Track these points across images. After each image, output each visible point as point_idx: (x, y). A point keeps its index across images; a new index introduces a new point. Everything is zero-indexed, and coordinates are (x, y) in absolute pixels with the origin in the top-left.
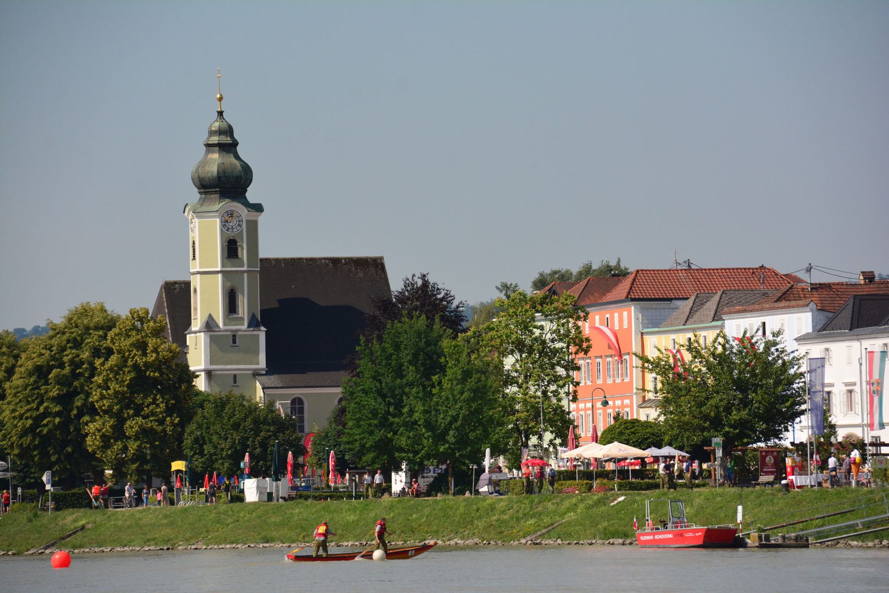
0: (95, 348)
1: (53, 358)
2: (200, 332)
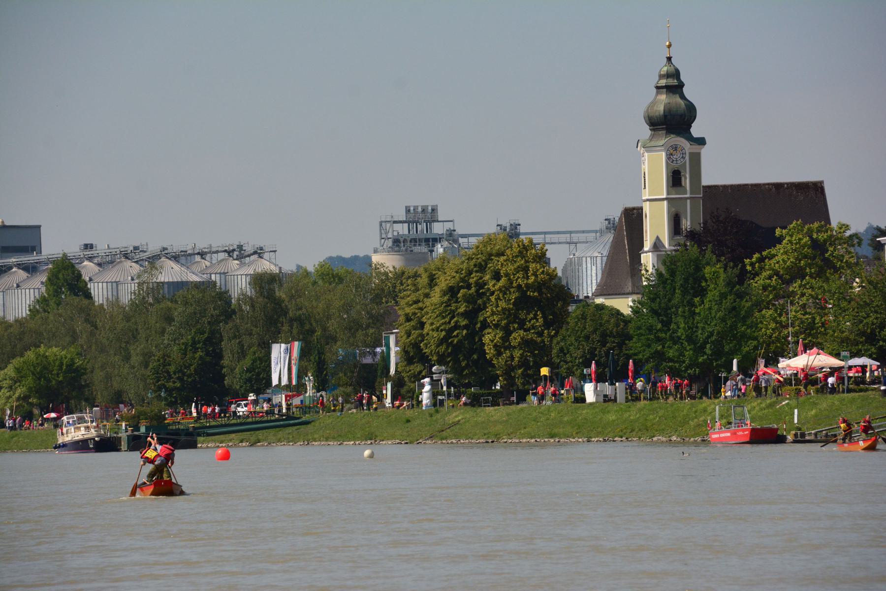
0: (495, 272)
1: (462, 280)
2: (649, 252)
